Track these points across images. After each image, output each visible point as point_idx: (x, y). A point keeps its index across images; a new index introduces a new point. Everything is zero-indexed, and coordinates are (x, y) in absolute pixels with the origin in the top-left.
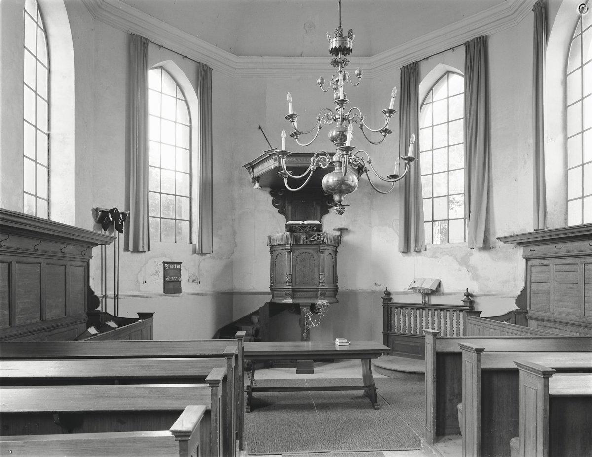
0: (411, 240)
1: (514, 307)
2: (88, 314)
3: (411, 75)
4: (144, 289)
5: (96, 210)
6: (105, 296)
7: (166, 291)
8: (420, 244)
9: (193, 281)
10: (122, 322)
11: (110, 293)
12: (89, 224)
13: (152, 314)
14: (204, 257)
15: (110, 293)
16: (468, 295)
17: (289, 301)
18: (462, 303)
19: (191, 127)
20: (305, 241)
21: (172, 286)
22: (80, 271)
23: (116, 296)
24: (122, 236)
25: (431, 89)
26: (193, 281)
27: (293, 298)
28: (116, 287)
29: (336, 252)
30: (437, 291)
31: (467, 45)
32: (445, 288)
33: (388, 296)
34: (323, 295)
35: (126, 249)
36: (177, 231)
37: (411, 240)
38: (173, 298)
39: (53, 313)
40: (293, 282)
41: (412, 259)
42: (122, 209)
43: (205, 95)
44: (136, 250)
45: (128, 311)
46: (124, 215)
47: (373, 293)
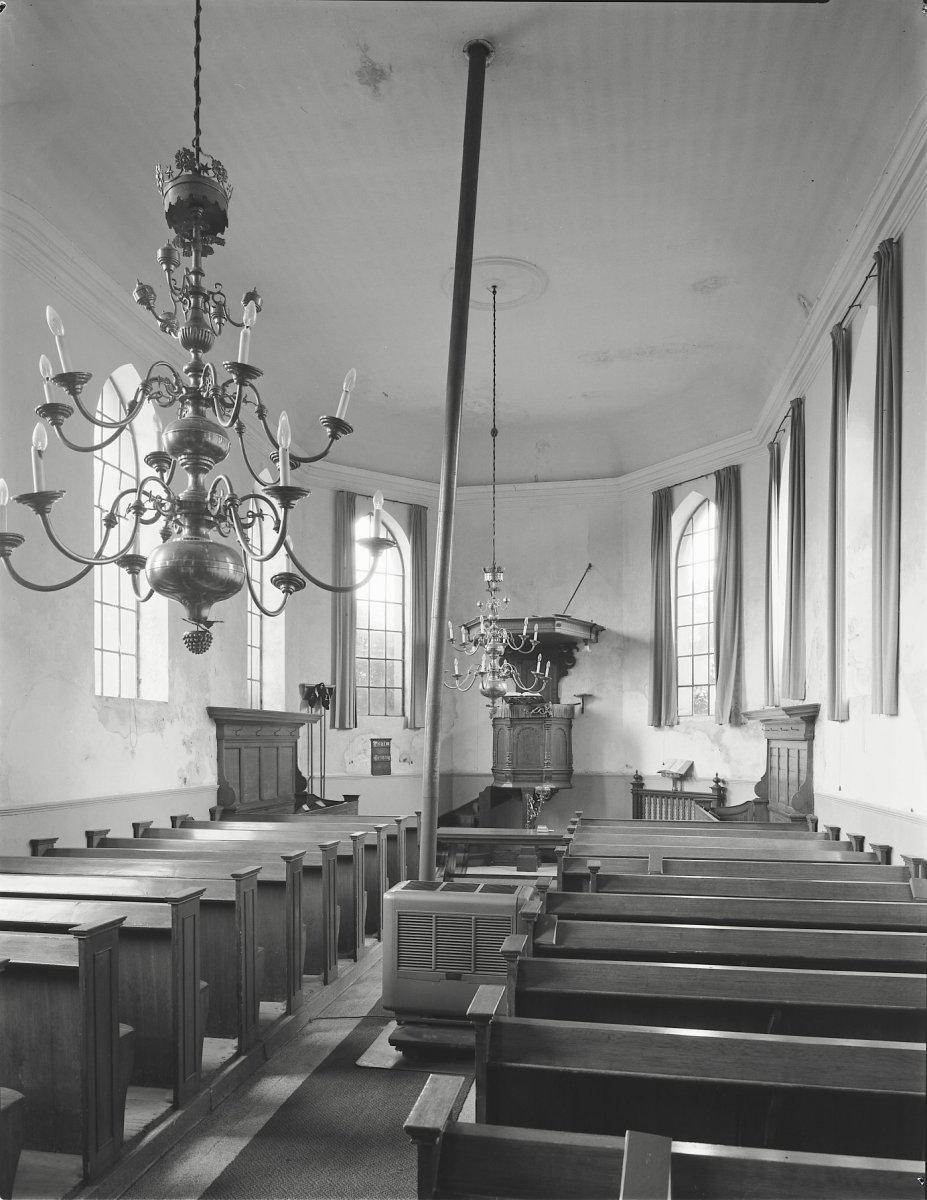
0: (661, 712)
1: (753, 796)
2: (296, 796)
3: (664, 503)
4: (351, 770)
5: (302, 686)
6: (311, 777)
7: (374, 772)
8: (672, 714)
9: (405, 760)
10: (329, 803)
11: (317, 774)
12: (297, 706)
13: (357, 797)
14: (417, 732)
15: (317, 774)
16: (717, 781)
17: (509, 785)
18: (710, 791)
19: (403, 577)
20: (527, 716)
21: (381, 767)
22: (288, 752)
23: (323, 777)
24: (328, 712)
25: (691, 518)
26: (405, 760)
27: (514, 781)
28: (323, 768)
29: (570, 726)
30: (688, 774)
31: (718, 474)
32: (698, 772)
33: (638, 782)
34: (549, 779)
35: (333, 726)
36: (389, 704)
37: (661, 712)
38: (382, 780)
39: (269, 794)
40: (515, 762)
41: (666, 735)
42: (328, 683)
43: (418, 535)
44: (342, 727)
45: (334, 794)
46: (331, 689)
47: (624, 776)
